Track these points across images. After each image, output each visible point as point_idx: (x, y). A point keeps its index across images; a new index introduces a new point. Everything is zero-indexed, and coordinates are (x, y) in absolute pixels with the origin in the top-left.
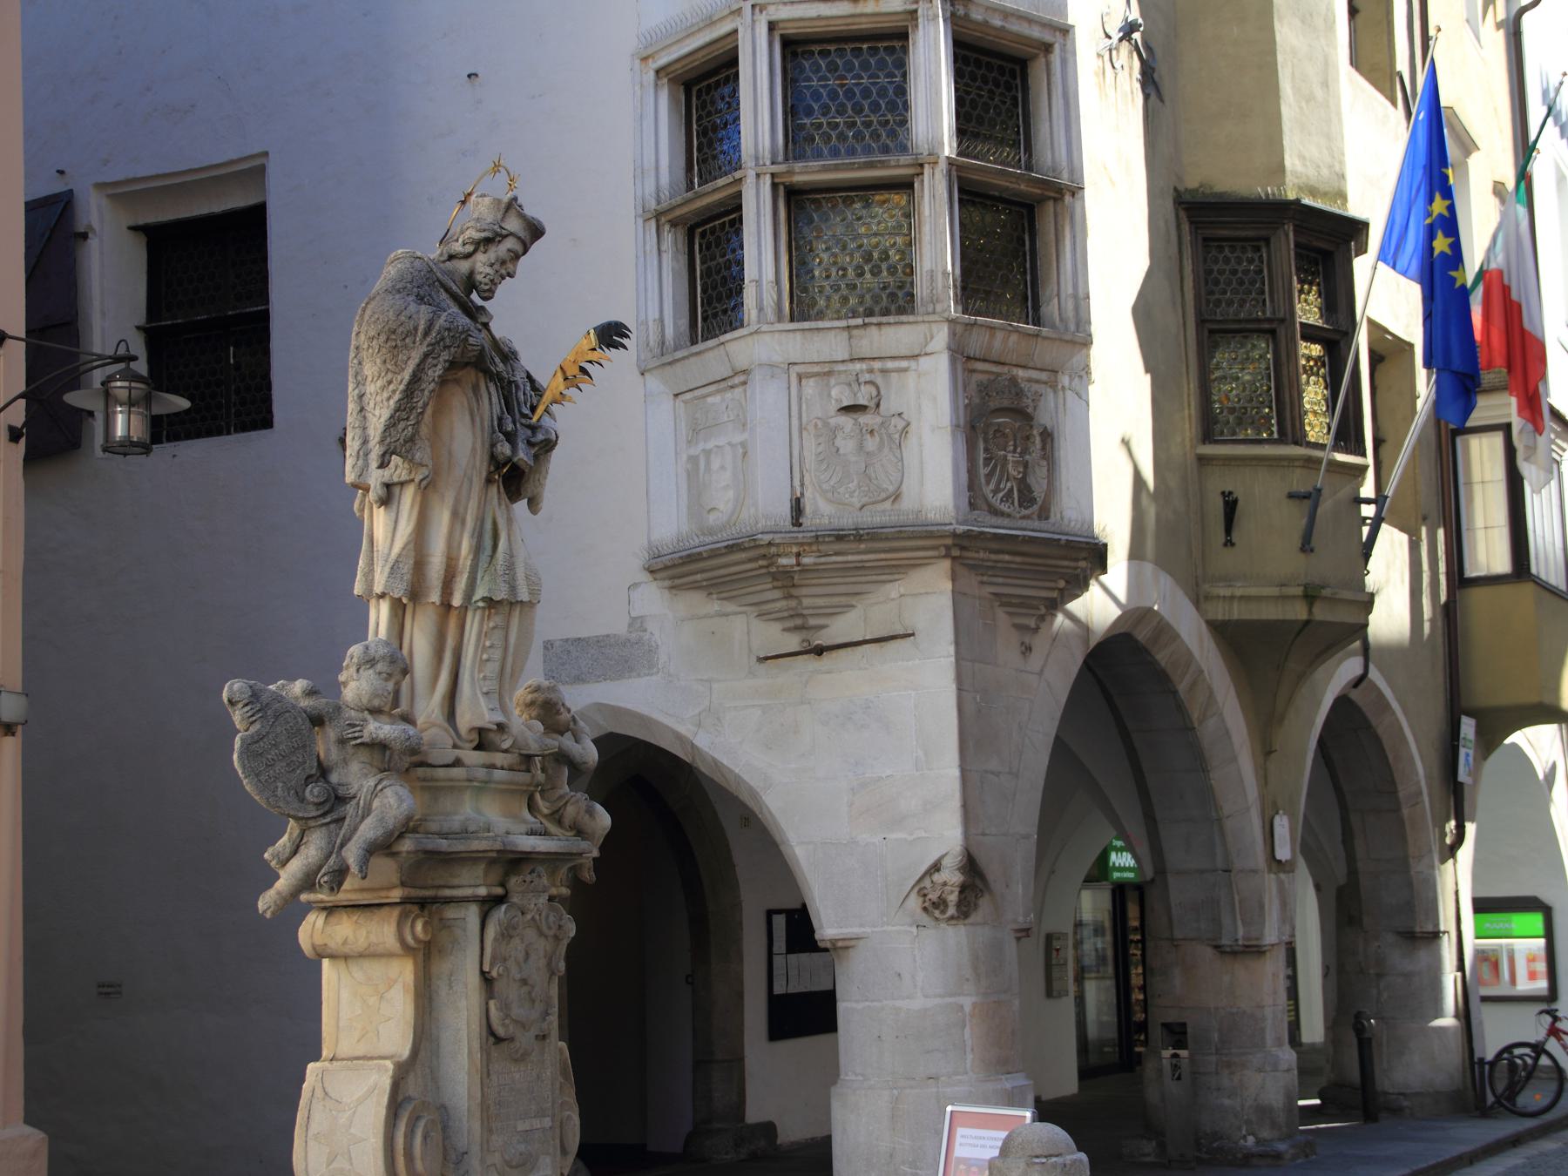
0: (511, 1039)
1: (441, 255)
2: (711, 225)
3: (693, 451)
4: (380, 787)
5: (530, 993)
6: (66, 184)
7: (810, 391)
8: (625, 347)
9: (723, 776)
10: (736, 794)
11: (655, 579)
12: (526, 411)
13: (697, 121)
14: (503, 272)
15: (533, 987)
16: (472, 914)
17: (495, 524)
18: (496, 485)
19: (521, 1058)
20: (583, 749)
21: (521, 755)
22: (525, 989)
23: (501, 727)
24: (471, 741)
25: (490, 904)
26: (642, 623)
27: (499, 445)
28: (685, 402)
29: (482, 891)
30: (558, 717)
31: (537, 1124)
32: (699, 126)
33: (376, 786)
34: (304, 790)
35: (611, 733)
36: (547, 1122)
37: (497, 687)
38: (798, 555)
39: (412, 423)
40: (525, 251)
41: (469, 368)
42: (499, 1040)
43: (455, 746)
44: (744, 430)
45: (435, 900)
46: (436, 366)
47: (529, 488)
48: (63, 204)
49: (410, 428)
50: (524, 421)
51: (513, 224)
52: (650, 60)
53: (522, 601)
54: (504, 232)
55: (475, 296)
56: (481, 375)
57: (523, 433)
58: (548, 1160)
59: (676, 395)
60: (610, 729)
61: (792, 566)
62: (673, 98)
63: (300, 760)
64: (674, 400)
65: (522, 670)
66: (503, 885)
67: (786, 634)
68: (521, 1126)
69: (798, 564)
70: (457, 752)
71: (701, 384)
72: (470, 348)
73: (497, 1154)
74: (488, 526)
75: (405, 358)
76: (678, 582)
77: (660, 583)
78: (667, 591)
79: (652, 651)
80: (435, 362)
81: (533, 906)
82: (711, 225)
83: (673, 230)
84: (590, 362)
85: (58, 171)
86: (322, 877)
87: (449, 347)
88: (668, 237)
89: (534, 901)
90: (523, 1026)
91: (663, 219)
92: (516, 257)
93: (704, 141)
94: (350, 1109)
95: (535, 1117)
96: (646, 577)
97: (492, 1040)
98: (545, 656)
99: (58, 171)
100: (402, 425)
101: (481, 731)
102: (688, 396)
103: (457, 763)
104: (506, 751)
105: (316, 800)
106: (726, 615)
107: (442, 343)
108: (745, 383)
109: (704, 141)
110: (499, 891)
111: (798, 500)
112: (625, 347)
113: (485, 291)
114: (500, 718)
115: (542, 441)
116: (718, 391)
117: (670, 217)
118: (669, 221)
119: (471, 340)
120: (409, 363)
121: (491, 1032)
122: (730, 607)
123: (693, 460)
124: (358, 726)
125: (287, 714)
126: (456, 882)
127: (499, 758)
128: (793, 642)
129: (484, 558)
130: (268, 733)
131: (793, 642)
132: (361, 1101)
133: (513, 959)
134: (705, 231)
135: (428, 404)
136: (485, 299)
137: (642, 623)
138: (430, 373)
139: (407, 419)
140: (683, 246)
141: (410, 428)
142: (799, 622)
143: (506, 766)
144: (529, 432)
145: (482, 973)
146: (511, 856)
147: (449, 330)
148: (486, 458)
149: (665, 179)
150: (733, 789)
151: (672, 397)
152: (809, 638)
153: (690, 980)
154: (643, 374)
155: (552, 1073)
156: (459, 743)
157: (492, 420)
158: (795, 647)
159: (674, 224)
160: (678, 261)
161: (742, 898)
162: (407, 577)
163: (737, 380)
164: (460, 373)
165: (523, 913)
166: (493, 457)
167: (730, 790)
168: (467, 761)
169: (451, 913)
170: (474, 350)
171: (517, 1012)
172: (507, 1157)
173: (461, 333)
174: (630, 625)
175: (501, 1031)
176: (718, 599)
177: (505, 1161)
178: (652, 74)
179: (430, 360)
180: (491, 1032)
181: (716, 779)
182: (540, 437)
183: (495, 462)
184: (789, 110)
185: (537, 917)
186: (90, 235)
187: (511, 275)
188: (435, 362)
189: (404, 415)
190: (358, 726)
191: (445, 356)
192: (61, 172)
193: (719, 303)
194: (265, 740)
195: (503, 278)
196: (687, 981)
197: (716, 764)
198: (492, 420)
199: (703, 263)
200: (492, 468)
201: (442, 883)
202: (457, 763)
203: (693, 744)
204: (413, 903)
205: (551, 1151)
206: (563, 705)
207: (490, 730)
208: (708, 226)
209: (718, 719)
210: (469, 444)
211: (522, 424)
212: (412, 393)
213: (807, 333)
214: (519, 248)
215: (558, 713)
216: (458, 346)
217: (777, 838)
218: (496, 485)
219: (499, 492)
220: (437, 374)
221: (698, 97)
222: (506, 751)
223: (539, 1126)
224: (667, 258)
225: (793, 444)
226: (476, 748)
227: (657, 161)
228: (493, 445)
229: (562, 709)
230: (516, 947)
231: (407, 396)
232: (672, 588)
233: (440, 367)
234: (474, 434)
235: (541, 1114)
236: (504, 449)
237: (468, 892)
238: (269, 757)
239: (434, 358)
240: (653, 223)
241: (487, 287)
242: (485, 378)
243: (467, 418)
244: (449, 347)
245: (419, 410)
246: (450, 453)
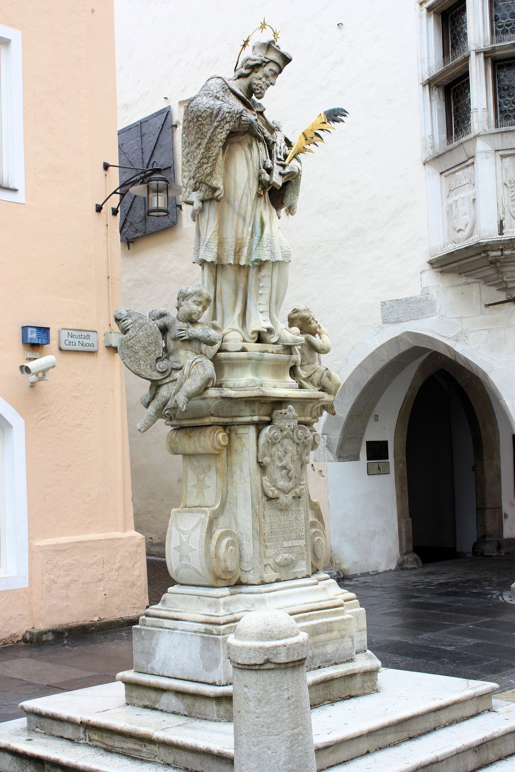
0: (277, 498)
1: (235, 76)
2: (458, 84)
3: (450, 201)
4: (194, 363)
5: (288, 474)
6: (168, 103)
7: (507, 164)
8: (343, 121)
9: (470, 365)
10: (477, 375)
11: (433, 268)
12: (282, 157)
13: (451, 32)
14: (268, 82)
15: (290, 471)
16: (252, 431)
17: (262, 219)
18: (263, 198)
19: (284, 509)
20: (323, 342)
21: (283, 345)
22: (284, 471)
23: (270, 331)
24: (254, 338)
25: (259, 426)
26: (427, 290)
27: (262, 176)
28: (445, 176)
29: (256, 418)
30: (310, 326)
31: (296, 543)
32: (451, 34)
33: (192, 362)
34: (156, 365)
35: (416, 346)
36: (302, 542)
37: (268, 309)
38: (502, 250)
39: (210, 165)
40: (281, 71)
41: (246, 135)
42: (269, 499)
43: (244, 341)
44: (473, 188)
45: (232, 424)
46: (222, 133)
47: (288, 201)
48: (167, 112)
49: (209, 168)
50: (278, 162)
51: (272, 56)
52: (424, 4)
53: (278, 261)
54: (267, 60)
55: (254, 97)
56: (253, 138)
57: (277, 169)
58: (304, 563)
59: (441, 173)
60: (415, 345)
61: (499, 256)
62: (436, 20)
63: (153, 349)
64: (440, 177)
65: (283, 300)
66: (270, 415)
67: (499, 292)
68: (286, 544)
69: (502, 255)
70: (244, 344)
71: (452, 166)
72: (243, 123)
73: (271, 559)
74: (258, 220)
75: (206, 130)
76: (444, 268)
77: (436, 270)
78: (439, 274)
79: (432, 304)
80: (221, 131)
81: (287, 427)
82: (458, 84)
83: (437, 89)
84: (322, 130)
85: (164, 98)
86: (165, 411)
87: (229, 122)
88: (435, 93)
89: (288, 424)
90: (285, 492)
91: (432, 85)
92: (276, 74)
93: (454, 41)
94: (189, 534)
95: (295, 539)
96: (428, 266)
97: (265, 499)
98: (382, 309)
99: (164, 98)
100: (205, 166)
101: (259, 333)
102: (447, 173)
103: (243, 350)
104: (275, 343)
105: (161, 370)
106: (469, 284)
107: (225, 120)
108: (473, 163)
109: (454, 41)
110: (267, 419)
111: (501, 222)
112: (343, 121)
113: (258, 94)
114: (269, 325)
115: (288, 173)
116: (461, 169)
117: (435, 83)
118: (436, 84)
119: (243, 118)
120: (208, 132)
121: (266, 495)
122: (471, 280)
123: (450, 206)
124: (183, 330)
125: (146, 326)
126: (243, 414)
127: (270, 347)
128: (503, 297)
129: (256, 238)
130: (135, 335)
131: (503, 297)
132: (193, 529)
133: (276, 455)
134: (456, 88)
135: (218, 154)
136: (259, 98)
137: (427, 290)
138: (219, 137)
139: (207, 163)
140: (442, 97)
141: (209, 168)
142: (504, 285)
143: (274, 352)
144: (281, 168)
145: (259, 463)
146: (272, 400)
147: (229, 112)
148: (256, 183)
149: (433, 62)
150: (475, 372)
151: (439, 174)
152: (511, 293)
153: (474, 469)
154: (424, 164)
155: (305, 516)
156: (247, 339)
157: (259, 163)
158: (504, 298)
159: (437, 86)
160: (440, 104)
161: (499, 429)
162: (215, 250)
163: (469, 162)
164: (241, 138)
165: (281, 431)
166: (260, 182)
167: (474, 373)
168: (248, 348)
169: (241, 430)
170: (246, 124)
171: (282, 483)
172: (277, 561)
173: (236, 114)
174: (422, 291)
175: (270, 494)
176: (464, 276)
177: (276, 563)
178: (425, 11)
179: (218, 130)
180: (266, 495)
181: (466, 368)
182: (287, 170)
183: (263, 185)
184: (493, 18)
185: (291, 433)
186: (178, 126)
187: (272, 84)
188: (221, 131)
189: (205, 161)
190: (183, 330)
191: (227, 126)
192: (166, 98)
193: (462, 124)
194: (132, 341)
195: (268, 86)
196: (473, 470)
197: (467, 360)
198: (259, 163)
199: (455, 105)
200: (260, 189)
201: (236, 414)
202: (243, 350)
203: (454, 350)
204: (219, 425)
205: (305, 557)
206: (313, 319)
207: (264, 332)
208: (456, 86)
209: (466, 337)
210: (246, 175)
211: (277, 164)
212: (209, 148)
213: (505, 135)
214: (275, 68)
215: (310, 323)
216: (235, 122)
217: (498, 397)
218: (263, 198)
219: (265, 202)
220: (222, 137)
221: (451, 20)
222: (275, 343)
223: (297, 545)
224: (435, 103)
225: (450, 170)
226: (256, 342)
227: (428, 54)
228: (260, 176)
229: (312, 321)
230: (278, 451)
231: (207, 150)
232: (441, 272)
233: (224, 133)
234: (248, 170)
235: (299, 538)
236: (267, 177)
237: (248, 419)
238: (137, 348)
239: (220, 129)
240: (427, 87)
241: (259, 91)
242: (256, 141)
243: (245, 161)
244: (229, 122)
245: (214, 158)
246: (235, 182)
